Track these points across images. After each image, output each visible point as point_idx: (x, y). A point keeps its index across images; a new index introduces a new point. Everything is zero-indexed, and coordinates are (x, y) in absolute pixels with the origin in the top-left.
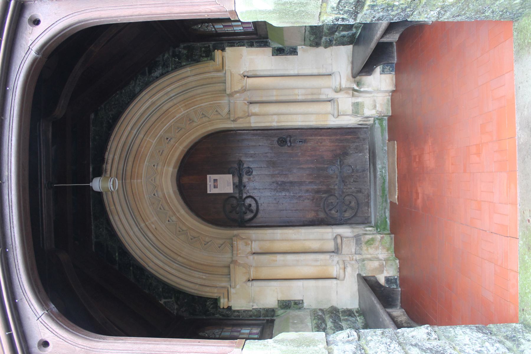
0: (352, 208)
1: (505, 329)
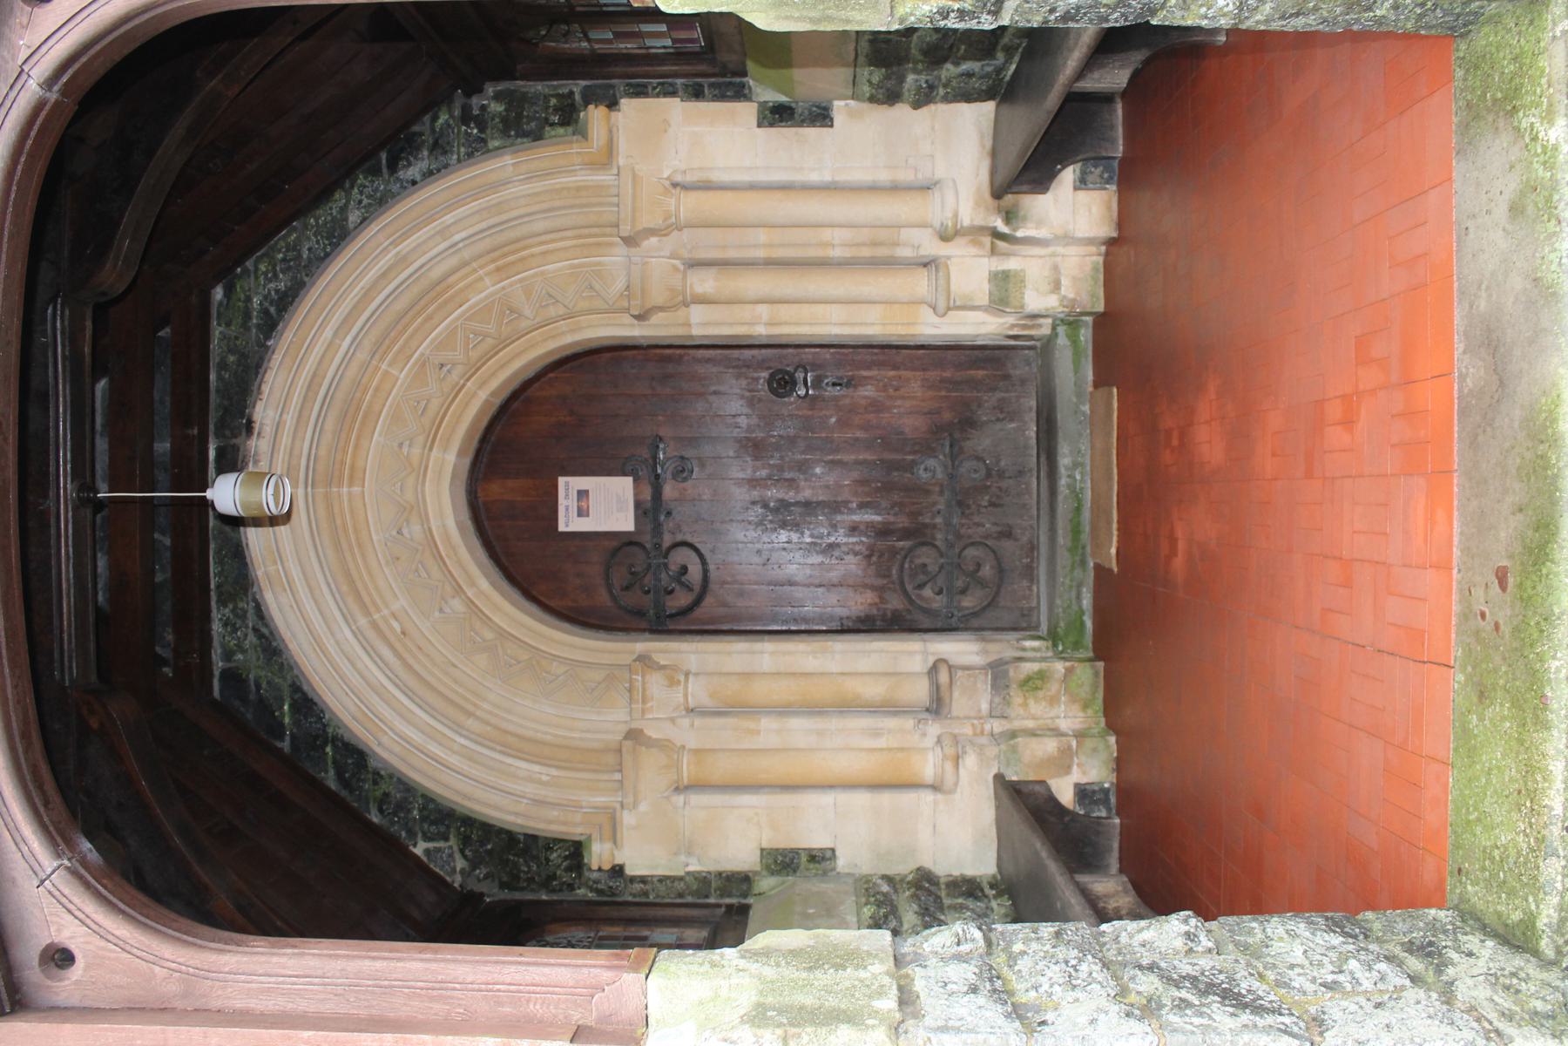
0: (982, 583)
1: (1405, 925)
